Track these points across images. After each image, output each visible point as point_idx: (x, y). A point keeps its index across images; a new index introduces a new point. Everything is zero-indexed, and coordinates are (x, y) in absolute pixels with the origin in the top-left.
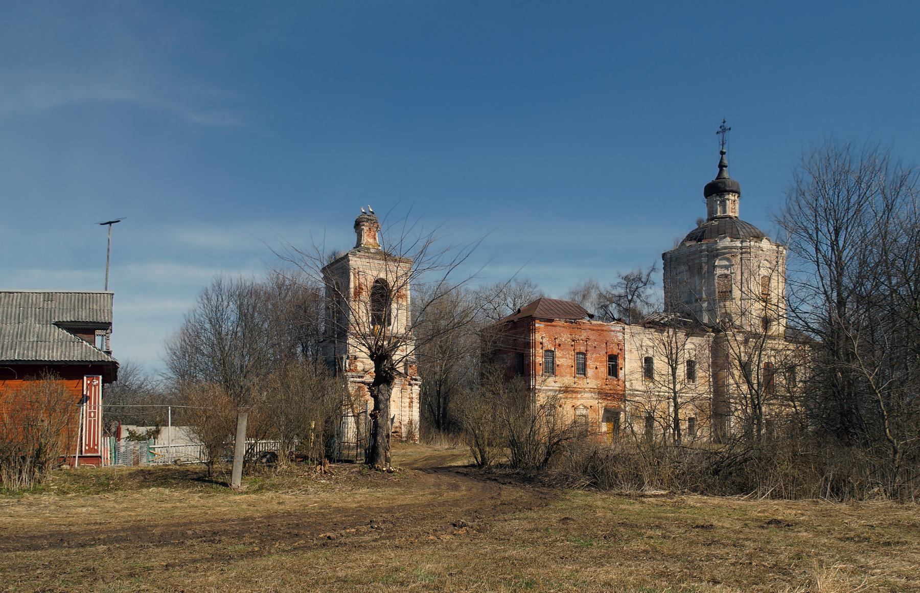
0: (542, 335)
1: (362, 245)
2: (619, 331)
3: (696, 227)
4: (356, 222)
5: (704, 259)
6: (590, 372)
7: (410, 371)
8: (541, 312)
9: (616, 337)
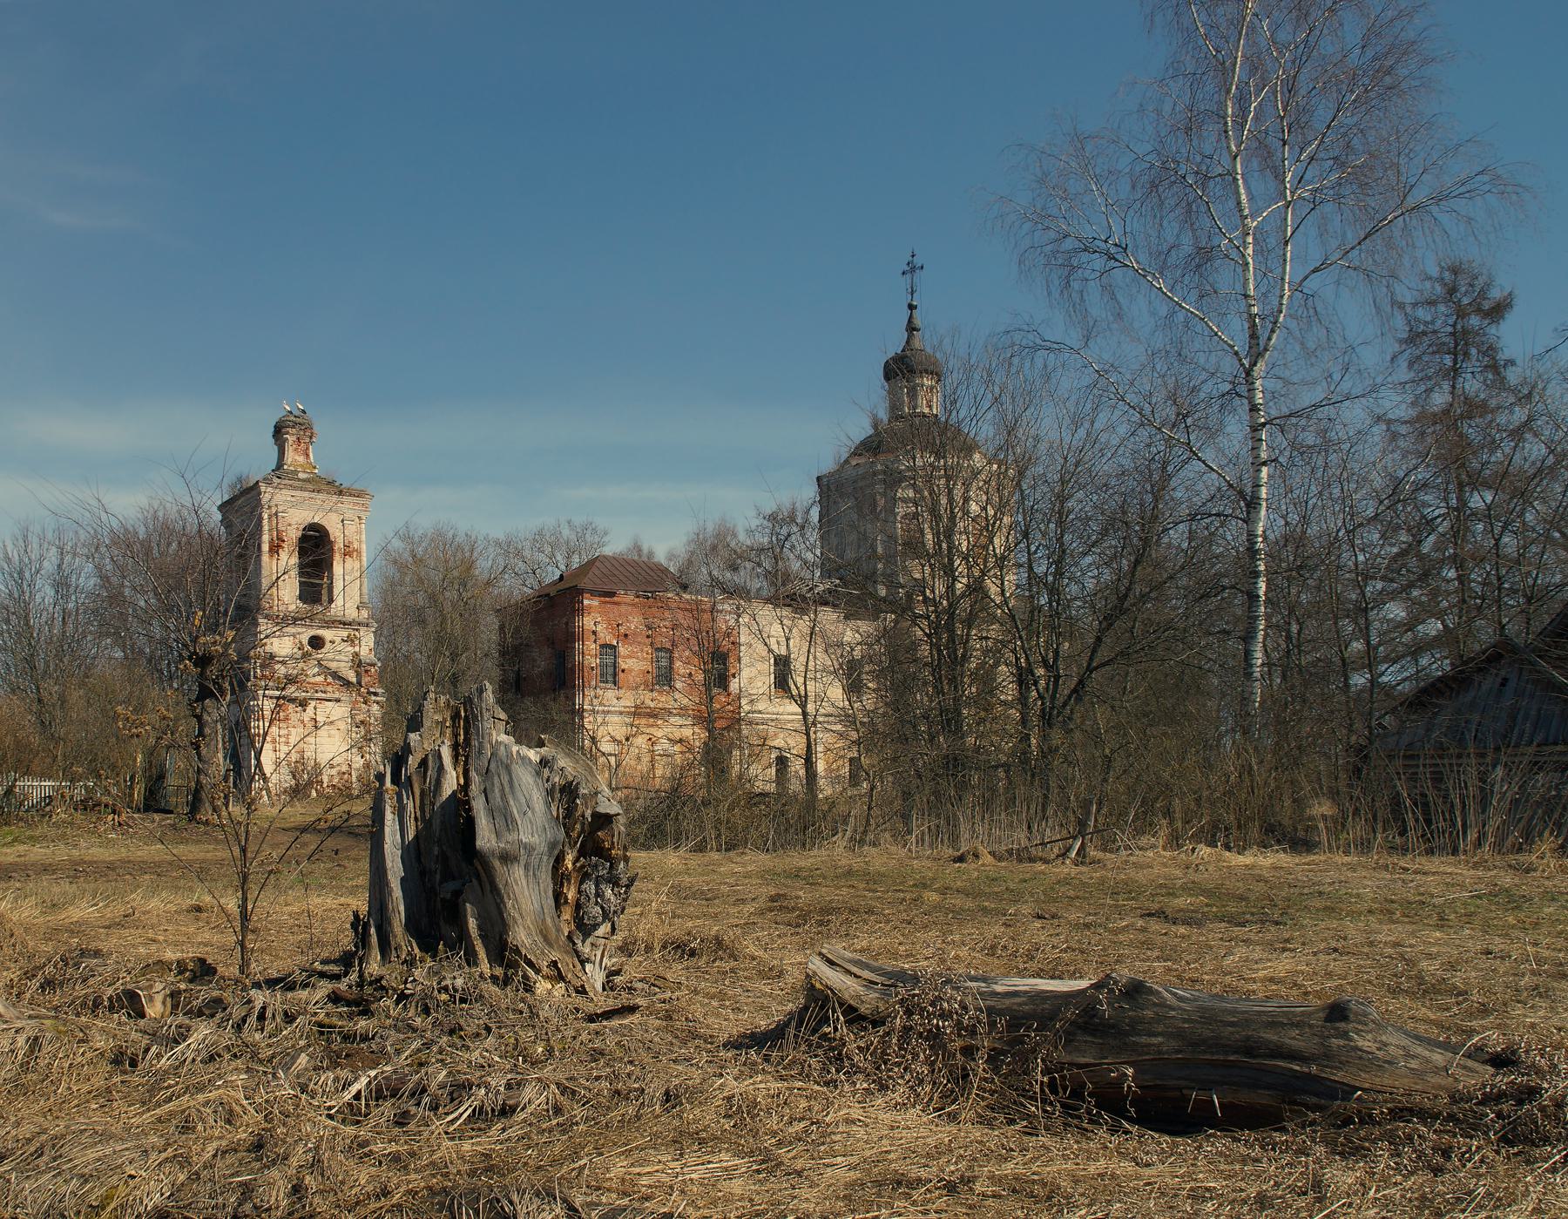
0: (594, 620)
1: (285, 467)
2: (730, 613)
3: (871, 432)
4: (275, 427)
5: (879, 488)
7: (365, 680)
8: (595, 579)
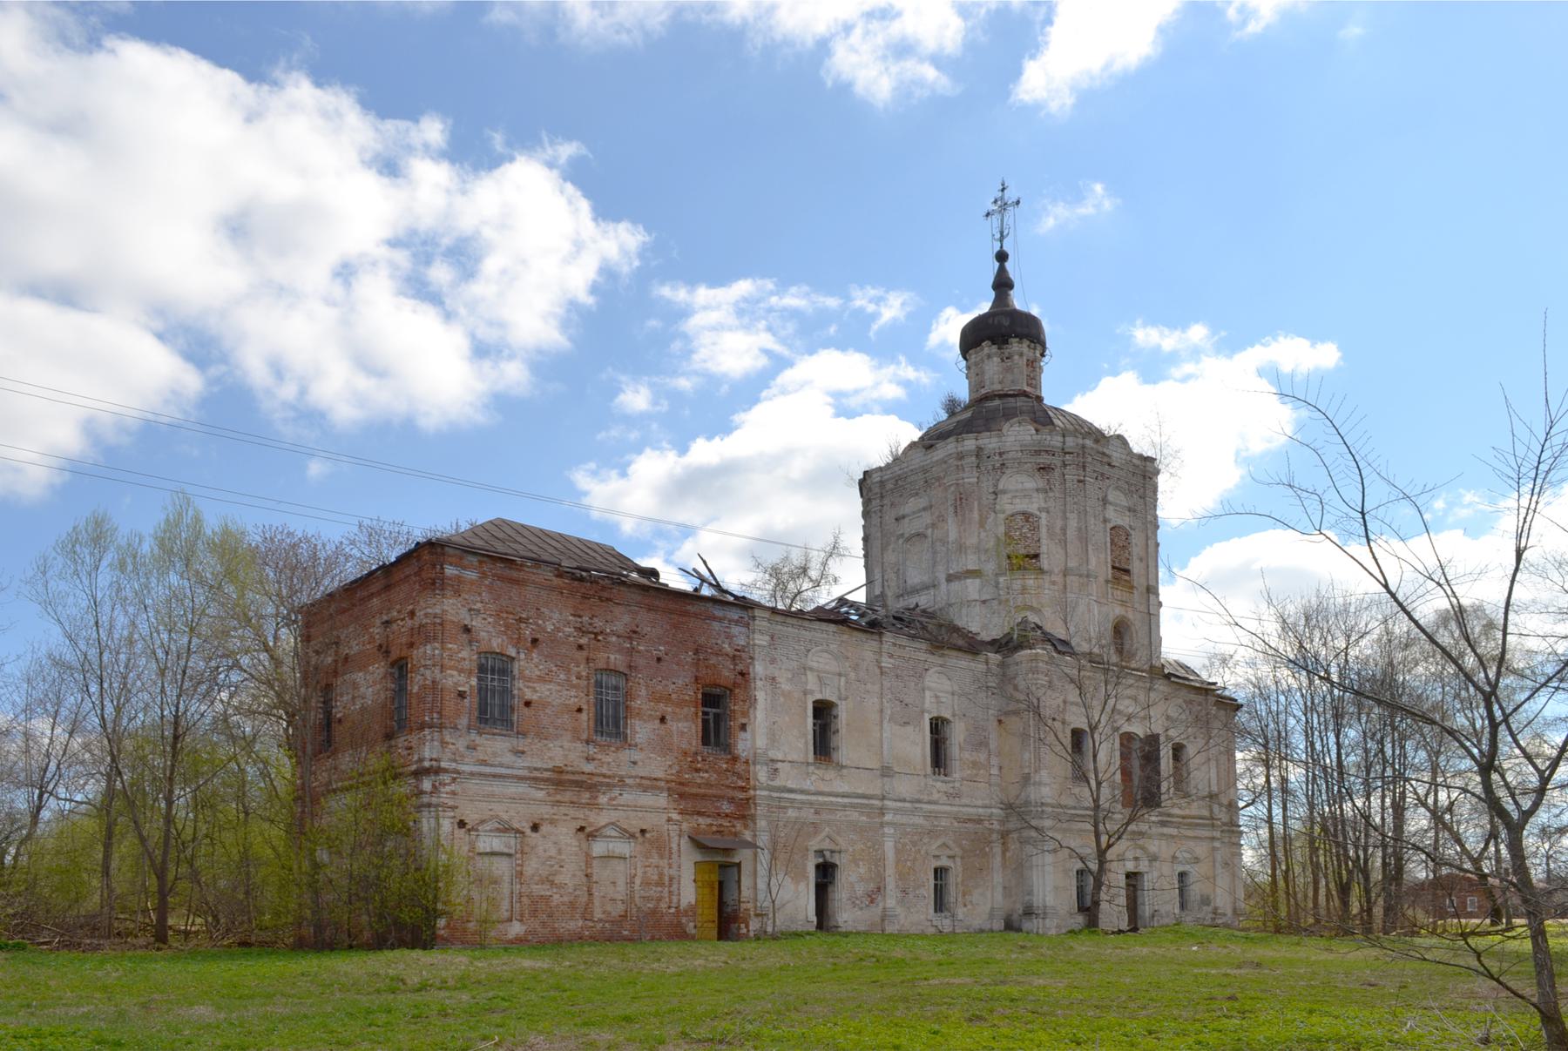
6: (642, 730)
9: (729, 637)
